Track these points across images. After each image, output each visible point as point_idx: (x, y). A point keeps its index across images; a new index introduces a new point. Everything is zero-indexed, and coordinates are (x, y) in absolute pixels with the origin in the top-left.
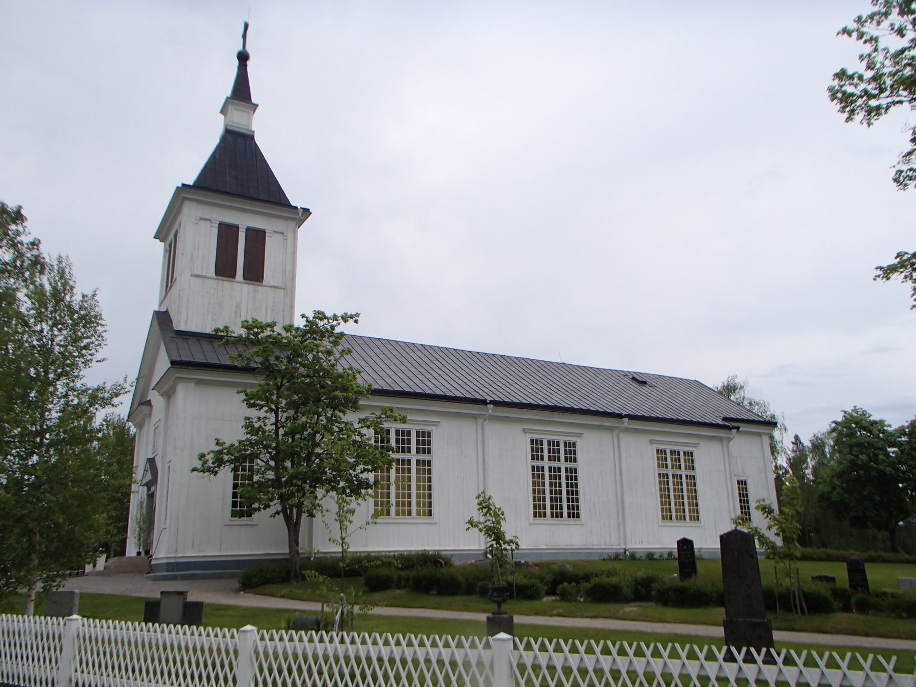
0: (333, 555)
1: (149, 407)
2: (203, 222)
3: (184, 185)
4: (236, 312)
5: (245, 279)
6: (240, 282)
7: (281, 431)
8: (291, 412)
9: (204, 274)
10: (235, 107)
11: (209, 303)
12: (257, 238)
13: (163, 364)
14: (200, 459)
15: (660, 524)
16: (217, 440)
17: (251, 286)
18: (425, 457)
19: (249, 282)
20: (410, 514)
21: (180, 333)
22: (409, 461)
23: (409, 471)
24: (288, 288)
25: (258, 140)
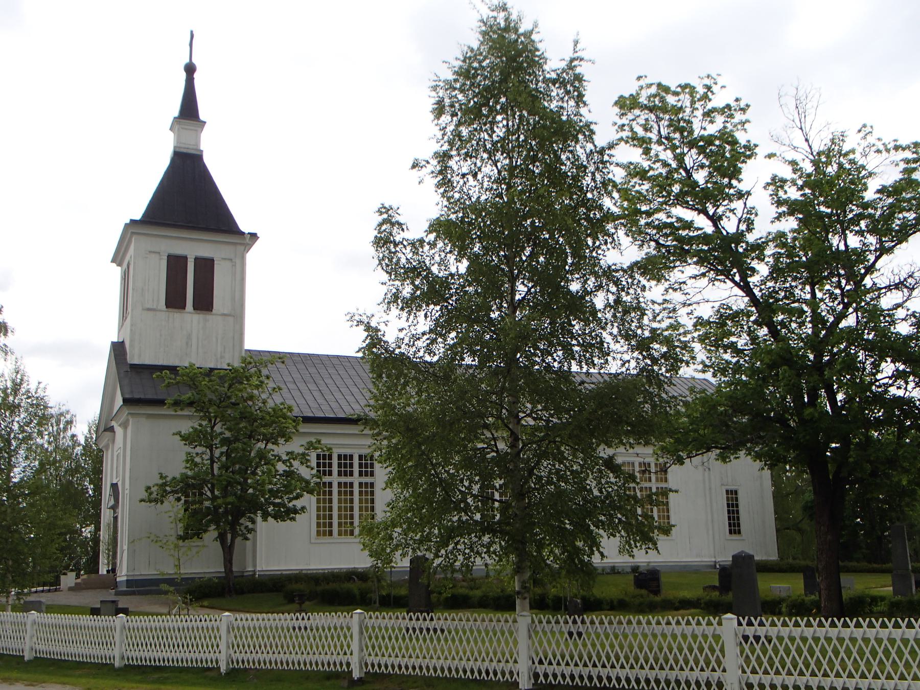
0: (284, 573)
1: (112, 433)
2: (153, 255)
3: (132, 221)
4: (187, 344)
5: (167, 307)
6: (190, 313)
7: (216, 466)
8: (224, 449)
9: (155, 307)
10: (183, 126)
11: (161, 336)
12: (205, 267)
13: (119, 401)
14: (146, 491)
15: (313, 541)
16: (161, 474)
17: (201, 316)
18: (368, 480)
19: (199, 312)
20: (331, 534)
21: (134, 367)
22: (351, 484)
23: (352, 493)
24: (237, 315)
25: (208, 160)
